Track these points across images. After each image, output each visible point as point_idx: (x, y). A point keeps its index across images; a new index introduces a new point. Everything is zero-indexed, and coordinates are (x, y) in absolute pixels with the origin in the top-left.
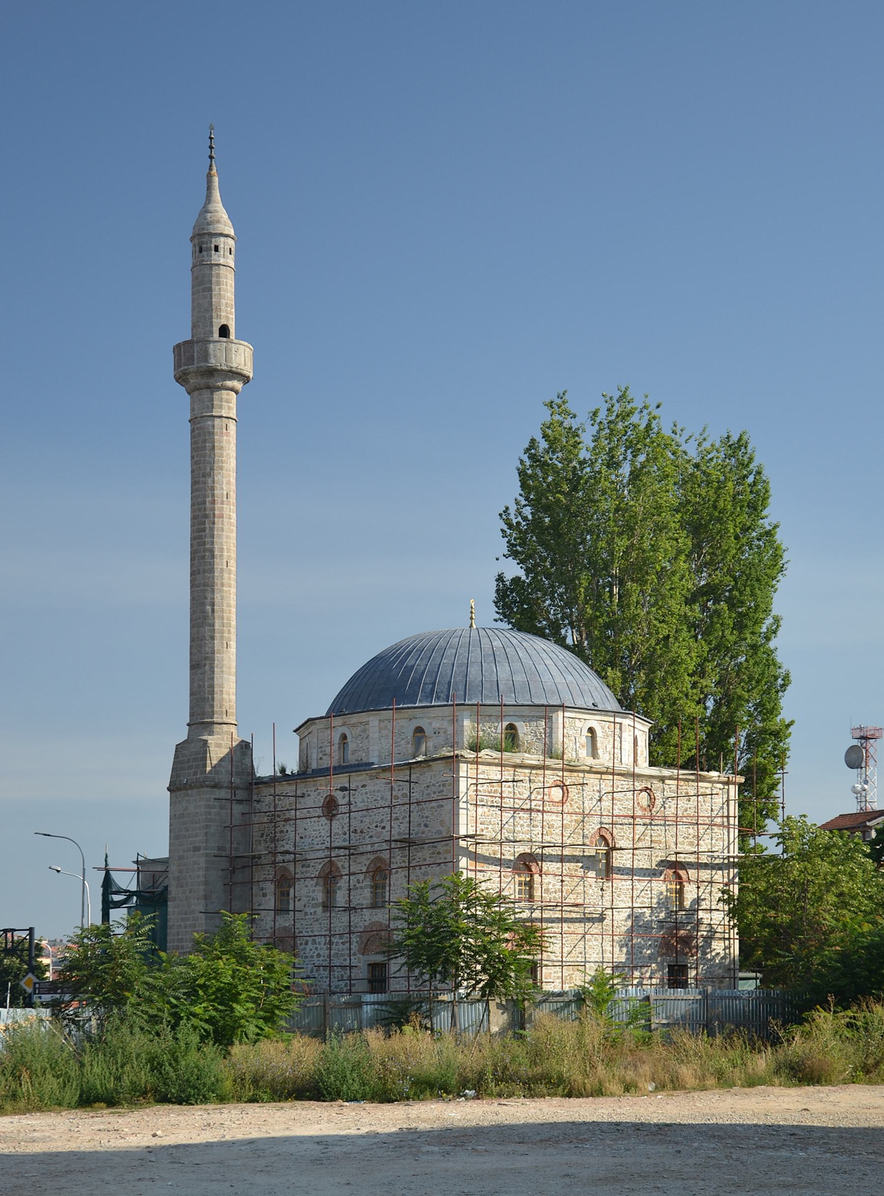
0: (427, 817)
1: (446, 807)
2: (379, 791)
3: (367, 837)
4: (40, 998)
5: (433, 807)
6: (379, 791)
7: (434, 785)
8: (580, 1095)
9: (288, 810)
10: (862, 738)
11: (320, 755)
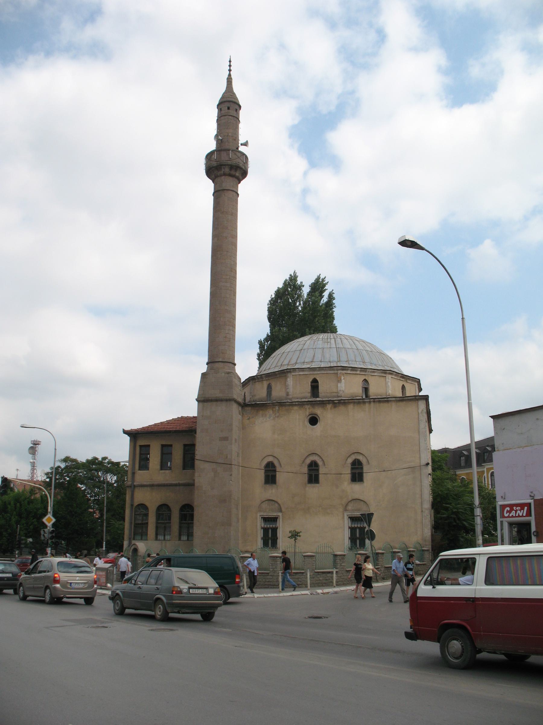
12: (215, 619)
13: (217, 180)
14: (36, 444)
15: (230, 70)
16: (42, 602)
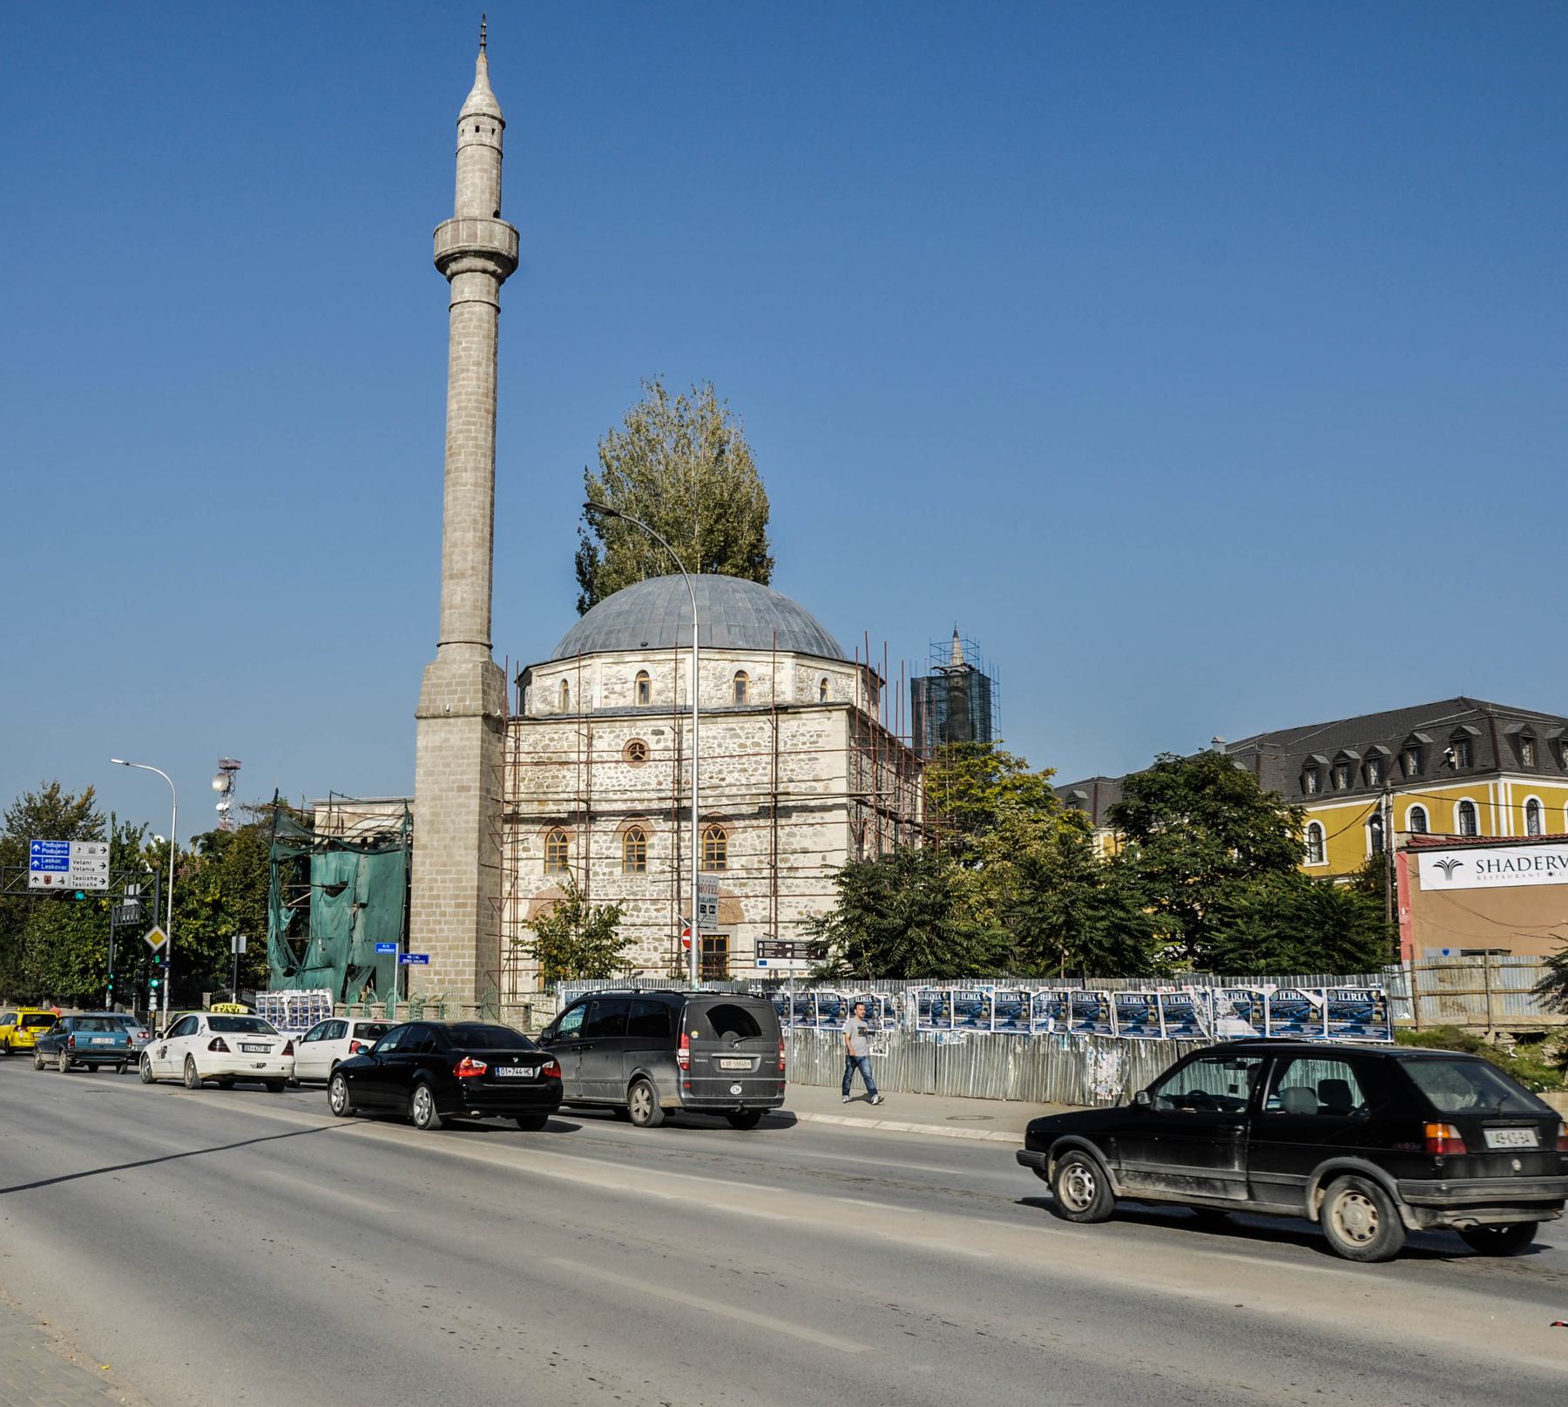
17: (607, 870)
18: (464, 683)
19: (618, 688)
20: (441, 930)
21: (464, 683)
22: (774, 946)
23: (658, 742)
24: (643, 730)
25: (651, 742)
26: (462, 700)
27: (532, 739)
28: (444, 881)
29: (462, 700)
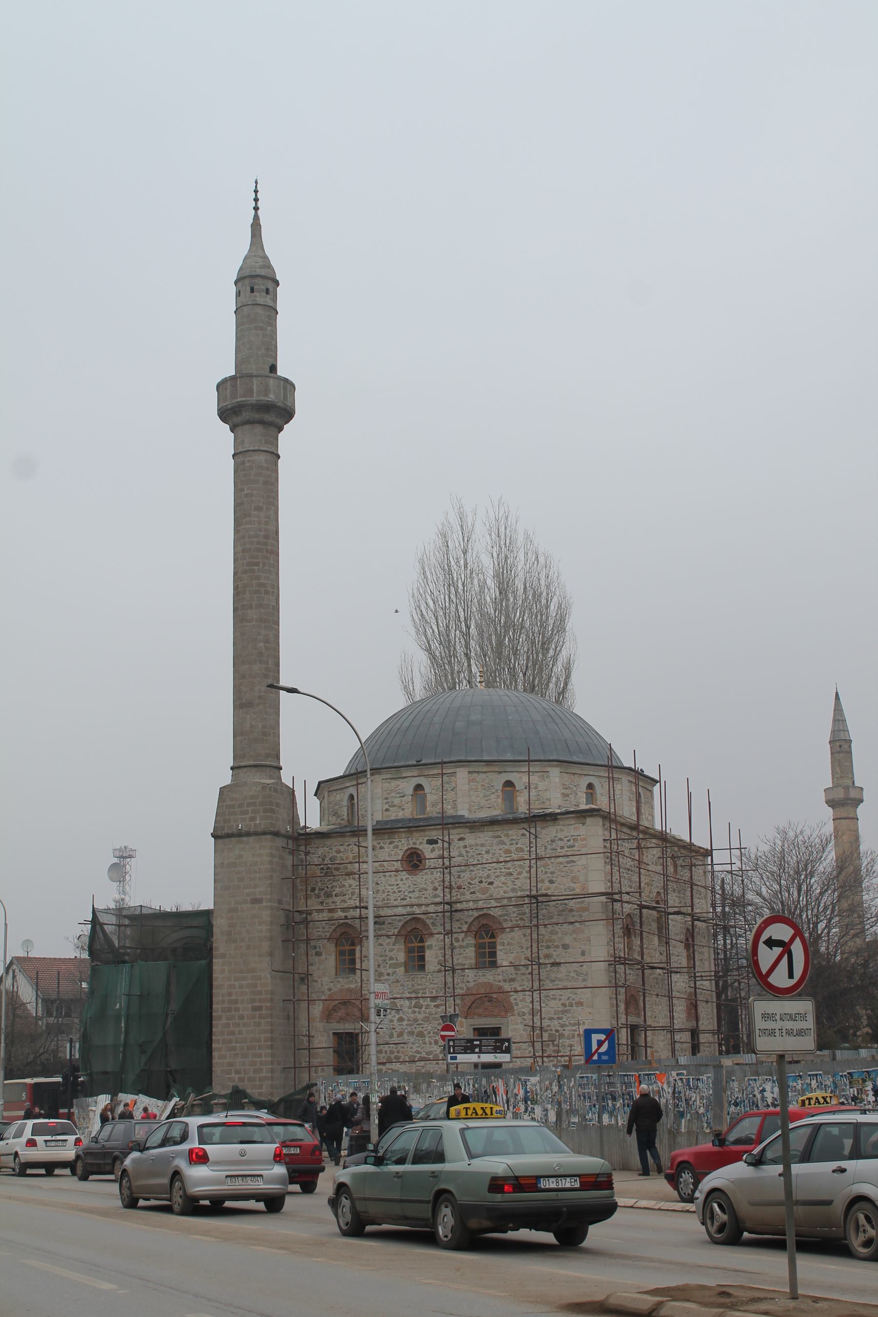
0: (552, 873)
1: (579, 863)
2: (482, 845)
3: (467, 893)
4: (455, 1058)
5: (561, 863)
6: (482, 845)
7: (561, 839)
8: (629, 1170)
9: (351, 863)
10: (121, 857)
11: (386, 806)
12: (285, 1208)
13: (239, 430)
14: (124, 856)
15: (256, 209)
16: (428, 1238)
17: (390, 971)
18: (254, 804)
19: (397, 801)
20: (240, 1033)
21: (254, 804)
22: (463, 1043)
23: (433, 850)
24: (419, 842)
25: (427, 850)
26: (253, 819)
27: (320, 851)
28: (241, 987)
29: (253, 819)
